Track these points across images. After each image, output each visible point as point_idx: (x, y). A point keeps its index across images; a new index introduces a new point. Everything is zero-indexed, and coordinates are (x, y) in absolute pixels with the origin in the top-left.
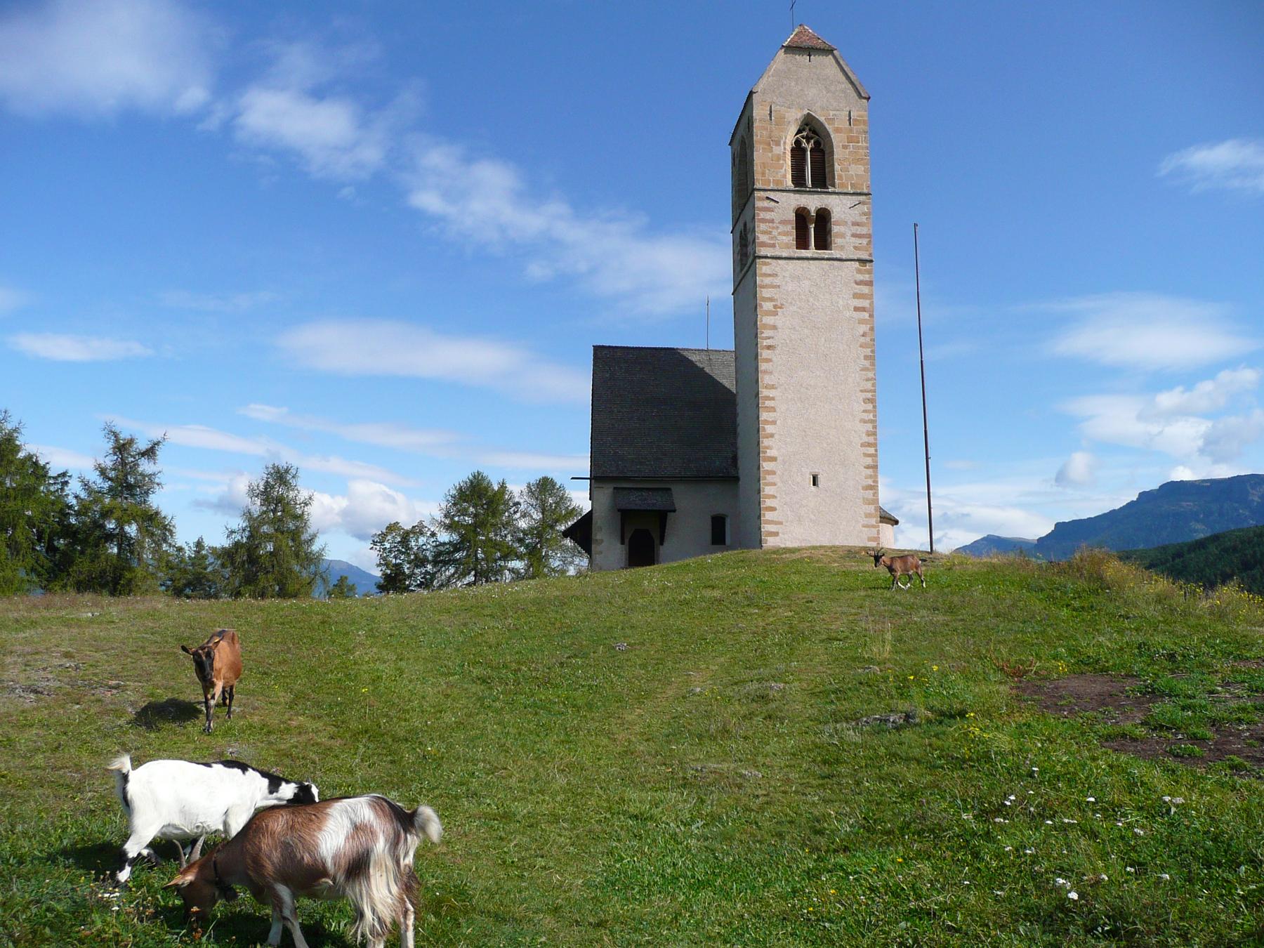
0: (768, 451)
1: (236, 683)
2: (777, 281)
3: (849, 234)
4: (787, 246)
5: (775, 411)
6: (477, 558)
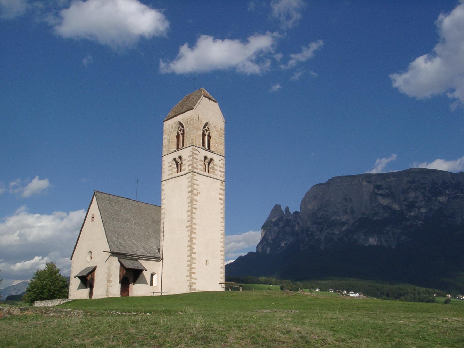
0: (194, 250)
1: (187, 160)
2: (198, 183)
3: (218, 170)
4: (201, 170)
5: (196, 234)
6: (68, 309)
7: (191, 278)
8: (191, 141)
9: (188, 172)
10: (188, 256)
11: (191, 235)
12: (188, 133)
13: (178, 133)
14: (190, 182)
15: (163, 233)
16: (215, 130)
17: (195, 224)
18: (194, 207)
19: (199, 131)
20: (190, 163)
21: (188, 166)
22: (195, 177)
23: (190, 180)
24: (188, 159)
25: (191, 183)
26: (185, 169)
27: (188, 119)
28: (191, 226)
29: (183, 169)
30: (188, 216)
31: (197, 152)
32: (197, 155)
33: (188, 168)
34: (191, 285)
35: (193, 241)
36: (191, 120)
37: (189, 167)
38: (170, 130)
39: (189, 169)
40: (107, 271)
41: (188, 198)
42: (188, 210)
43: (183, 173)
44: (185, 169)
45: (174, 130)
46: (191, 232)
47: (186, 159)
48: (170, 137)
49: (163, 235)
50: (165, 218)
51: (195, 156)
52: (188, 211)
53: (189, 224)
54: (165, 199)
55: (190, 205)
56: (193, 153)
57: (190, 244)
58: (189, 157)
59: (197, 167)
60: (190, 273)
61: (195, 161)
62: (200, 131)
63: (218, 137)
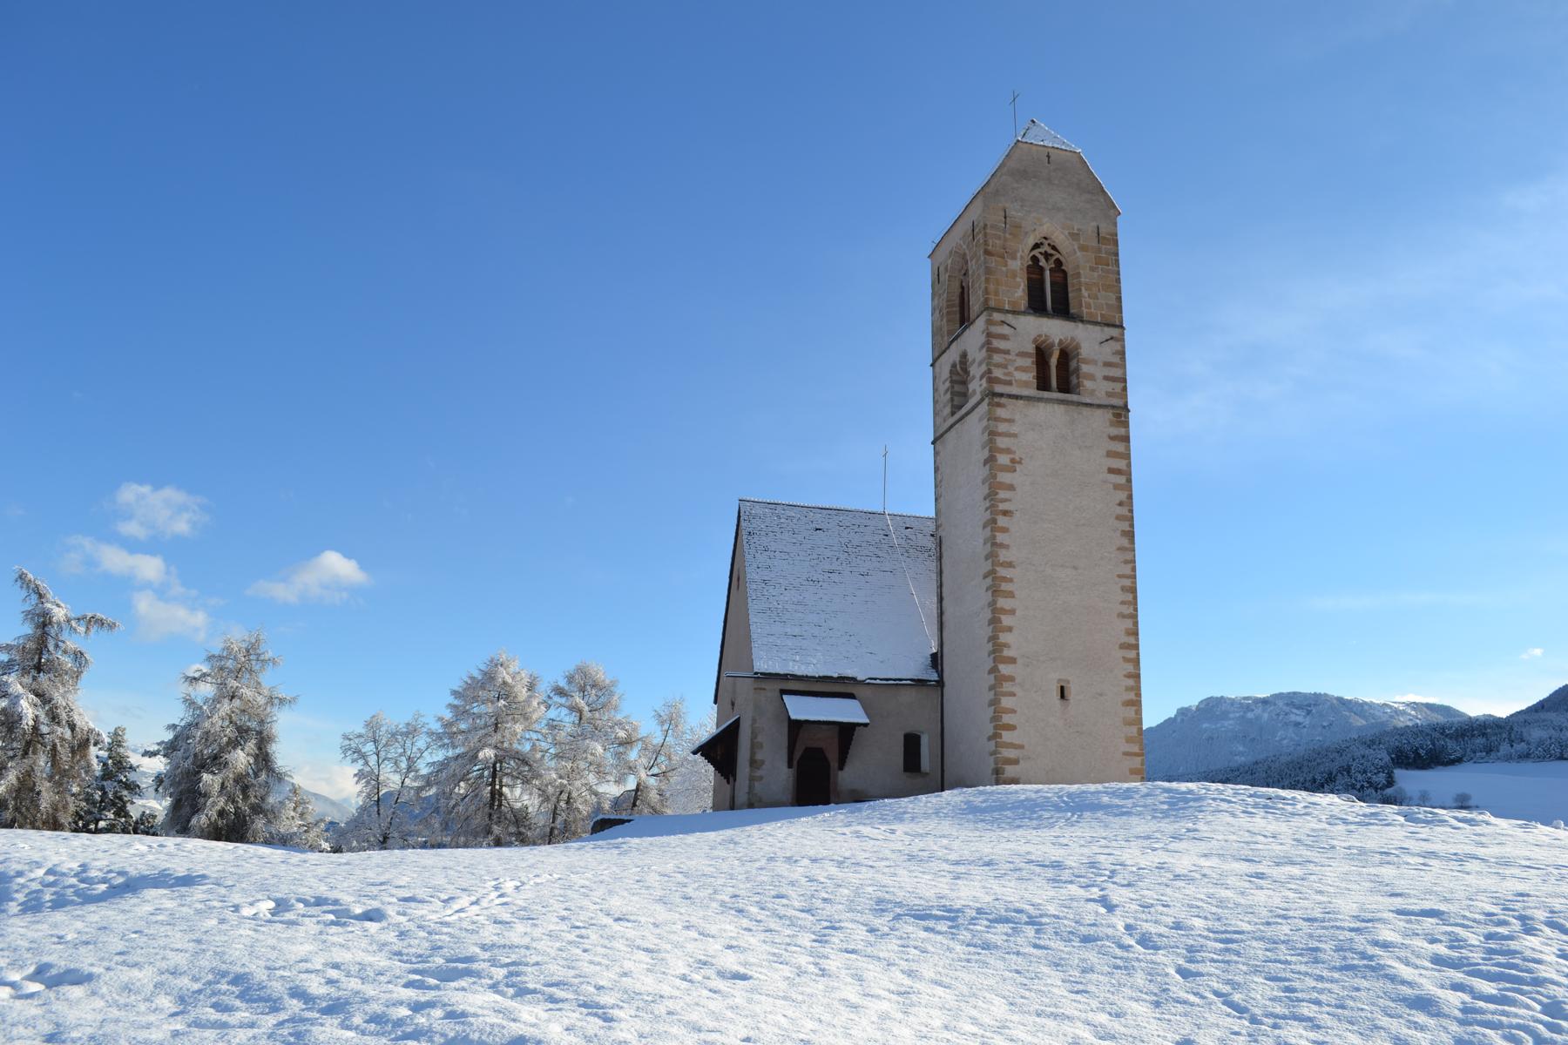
5: (1013, 597)
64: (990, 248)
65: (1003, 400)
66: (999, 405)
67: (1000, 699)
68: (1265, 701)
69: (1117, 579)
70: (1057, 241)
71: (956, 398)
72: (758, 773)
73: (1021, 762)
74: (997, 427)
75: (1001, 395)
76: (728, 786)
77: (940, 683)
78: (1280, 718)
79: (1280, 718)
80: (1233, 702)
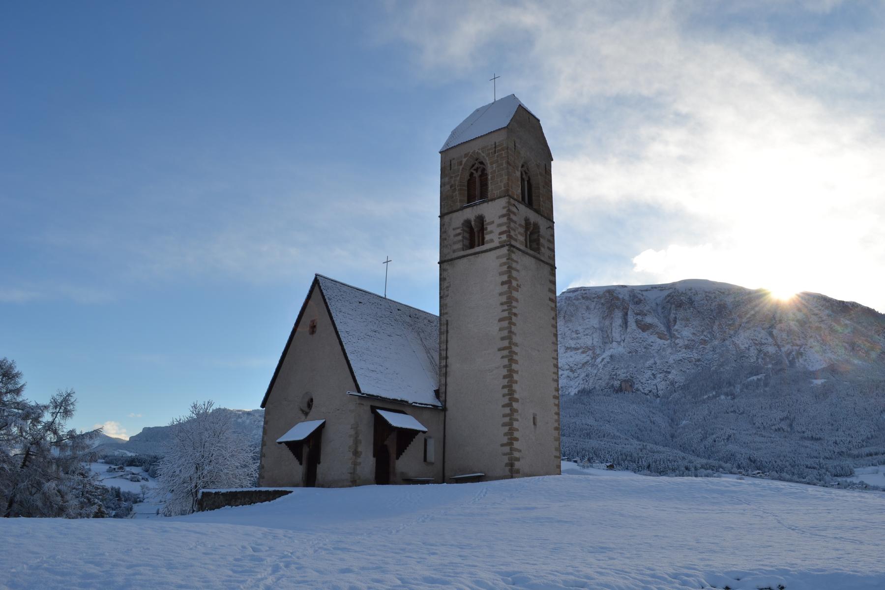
1: (495, 224)
3: (546, 247)
5: (517, 364)
7: (511, 449)
8: (503, 189)
9: (498, 245)
10: (504, 406)
11: (510, 365)
12: (497, 173)
13: (471, 174)
14: (504, 264)
15: (445, 361)
16: (538, 173)
17: (516, 345)
18: (513, 312)
19: (516, 172)
20: (504, 228)
21: (498, 234)
22: (514, 256)
23: (504, 260)
24: (498, 221)
25: (507, 265)
26: (492, 241)
27: (495, 147)
28: (510, 348)
29: (487, 241)
30: (501, 330)
31: (514, 209)
32: (514, 214)
33: (499, 238)
34: (513, 462)
35: (514, 377)
36: (503, 149)
37: (501, 236)
38: (456, 167)
39: (501, 240)
40: (352, 432)
41: (501, 294)
42: (501, 317)
43: (487, 246)
44: (492, 241)
45: (463, 168)
46: (509, 360)
47: (493, 222)
48: (455, 181)
49: (445, 364)
50: (449, 331)
51: (512, 216)
52: (500, 320)
53: (506, 343)
54: (447, 296)
55: (505, 307)
56: (509, 210)
57: (508, 383)
58: (499, 218)
59: (516, 237)
60: (509, 439)
61: (512, 225)
62: (518, 171)
63: (543, 186)
64: (509, 160)
65: (514, 250)
66: (513, 252)
67: (513, 423)
68: (249, 413)
69: (552, 360)
70: (530, 166)
71: (465, 240)
72: (359, 460)
73: (521, 460)
74: (512, 264)
75: (514, 247)
76: (301, 467)
77: (444, 409)
78: (256, 423)
79: (256, 423)
80: (231, 412)
